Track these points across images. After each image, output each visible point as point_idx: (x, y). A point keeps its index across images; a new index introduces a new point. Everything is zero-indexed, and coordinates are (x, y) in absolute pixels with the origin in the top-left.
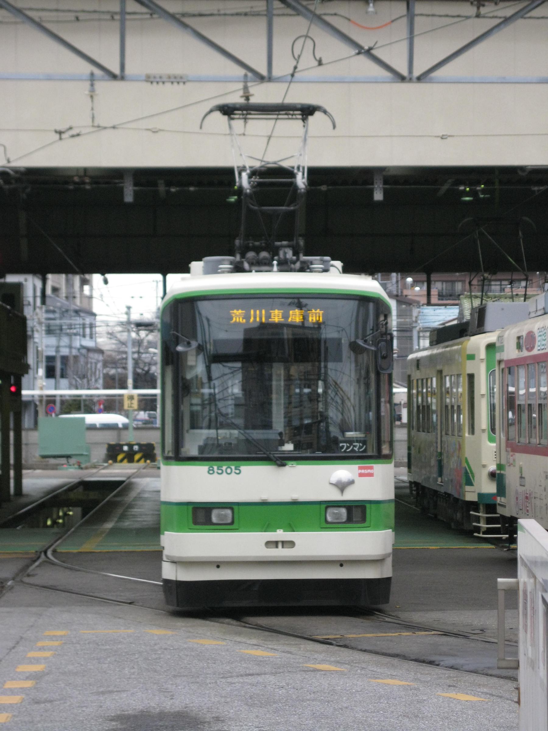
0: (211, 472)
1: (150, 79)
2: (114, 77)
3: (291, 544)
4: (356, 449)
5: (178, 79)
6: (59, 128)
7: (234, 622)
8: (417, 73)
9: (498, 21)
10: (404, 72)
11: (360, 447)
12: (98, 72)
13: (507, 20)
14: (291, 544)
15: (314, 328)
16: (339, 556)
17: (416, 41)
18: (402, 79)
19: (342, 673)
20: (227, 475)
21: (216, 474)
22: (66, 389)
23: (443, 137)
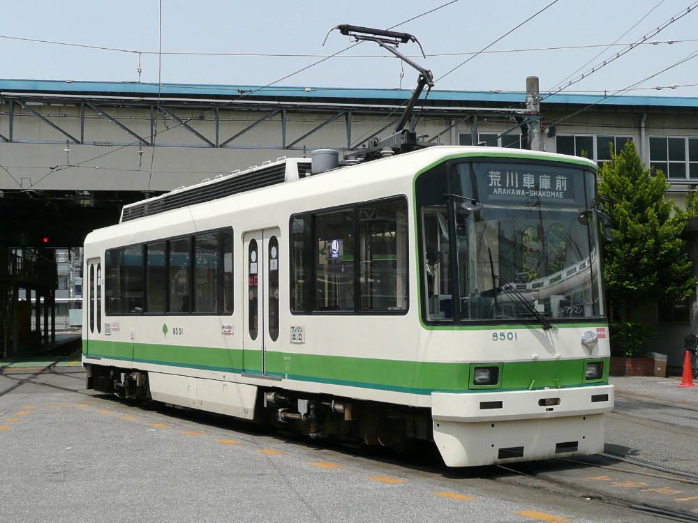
0: (495, 338)
1: (95, 144)
2: (78, 143)
3: (498, 405)
4: (576, 312)
5: (108, 144)
6: (52, 167)
7: (490, 481)
8: (220, 143)
9: (255, 122)
10: (215, 143)
11: (579, 310)
12: (70, 140)
13: (259, 121)
14: (498, 405)
15: (449, 223)
16: (538, 414)
17: (219, 126)
18: (214, 146)
19: (26, 397)
20: (503, 342)
21: (499, 340)
22: (467, 240)
23: (654, 43)
